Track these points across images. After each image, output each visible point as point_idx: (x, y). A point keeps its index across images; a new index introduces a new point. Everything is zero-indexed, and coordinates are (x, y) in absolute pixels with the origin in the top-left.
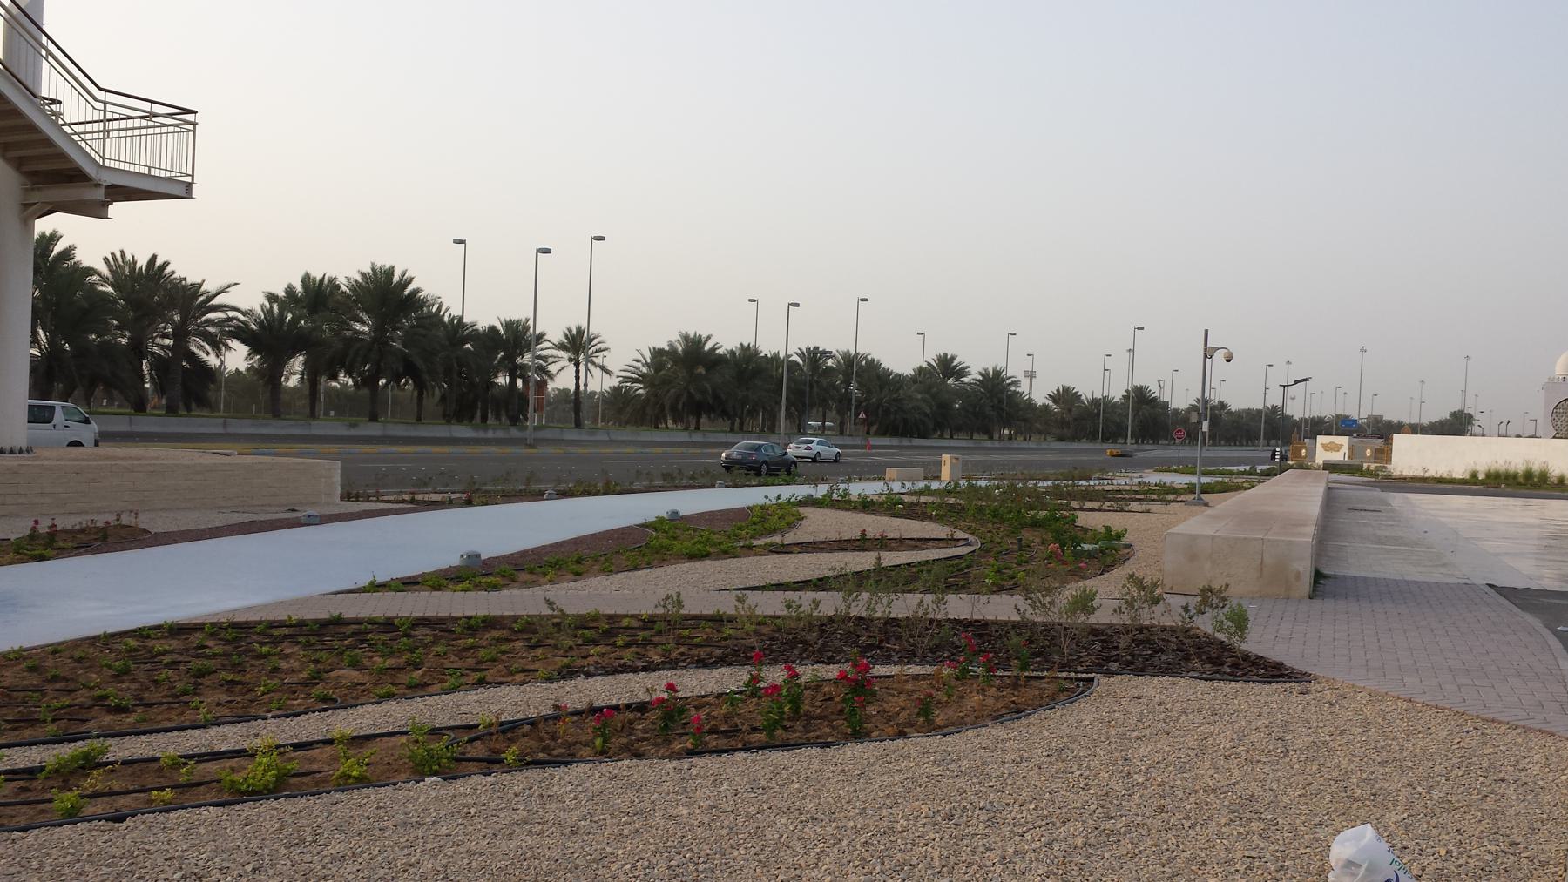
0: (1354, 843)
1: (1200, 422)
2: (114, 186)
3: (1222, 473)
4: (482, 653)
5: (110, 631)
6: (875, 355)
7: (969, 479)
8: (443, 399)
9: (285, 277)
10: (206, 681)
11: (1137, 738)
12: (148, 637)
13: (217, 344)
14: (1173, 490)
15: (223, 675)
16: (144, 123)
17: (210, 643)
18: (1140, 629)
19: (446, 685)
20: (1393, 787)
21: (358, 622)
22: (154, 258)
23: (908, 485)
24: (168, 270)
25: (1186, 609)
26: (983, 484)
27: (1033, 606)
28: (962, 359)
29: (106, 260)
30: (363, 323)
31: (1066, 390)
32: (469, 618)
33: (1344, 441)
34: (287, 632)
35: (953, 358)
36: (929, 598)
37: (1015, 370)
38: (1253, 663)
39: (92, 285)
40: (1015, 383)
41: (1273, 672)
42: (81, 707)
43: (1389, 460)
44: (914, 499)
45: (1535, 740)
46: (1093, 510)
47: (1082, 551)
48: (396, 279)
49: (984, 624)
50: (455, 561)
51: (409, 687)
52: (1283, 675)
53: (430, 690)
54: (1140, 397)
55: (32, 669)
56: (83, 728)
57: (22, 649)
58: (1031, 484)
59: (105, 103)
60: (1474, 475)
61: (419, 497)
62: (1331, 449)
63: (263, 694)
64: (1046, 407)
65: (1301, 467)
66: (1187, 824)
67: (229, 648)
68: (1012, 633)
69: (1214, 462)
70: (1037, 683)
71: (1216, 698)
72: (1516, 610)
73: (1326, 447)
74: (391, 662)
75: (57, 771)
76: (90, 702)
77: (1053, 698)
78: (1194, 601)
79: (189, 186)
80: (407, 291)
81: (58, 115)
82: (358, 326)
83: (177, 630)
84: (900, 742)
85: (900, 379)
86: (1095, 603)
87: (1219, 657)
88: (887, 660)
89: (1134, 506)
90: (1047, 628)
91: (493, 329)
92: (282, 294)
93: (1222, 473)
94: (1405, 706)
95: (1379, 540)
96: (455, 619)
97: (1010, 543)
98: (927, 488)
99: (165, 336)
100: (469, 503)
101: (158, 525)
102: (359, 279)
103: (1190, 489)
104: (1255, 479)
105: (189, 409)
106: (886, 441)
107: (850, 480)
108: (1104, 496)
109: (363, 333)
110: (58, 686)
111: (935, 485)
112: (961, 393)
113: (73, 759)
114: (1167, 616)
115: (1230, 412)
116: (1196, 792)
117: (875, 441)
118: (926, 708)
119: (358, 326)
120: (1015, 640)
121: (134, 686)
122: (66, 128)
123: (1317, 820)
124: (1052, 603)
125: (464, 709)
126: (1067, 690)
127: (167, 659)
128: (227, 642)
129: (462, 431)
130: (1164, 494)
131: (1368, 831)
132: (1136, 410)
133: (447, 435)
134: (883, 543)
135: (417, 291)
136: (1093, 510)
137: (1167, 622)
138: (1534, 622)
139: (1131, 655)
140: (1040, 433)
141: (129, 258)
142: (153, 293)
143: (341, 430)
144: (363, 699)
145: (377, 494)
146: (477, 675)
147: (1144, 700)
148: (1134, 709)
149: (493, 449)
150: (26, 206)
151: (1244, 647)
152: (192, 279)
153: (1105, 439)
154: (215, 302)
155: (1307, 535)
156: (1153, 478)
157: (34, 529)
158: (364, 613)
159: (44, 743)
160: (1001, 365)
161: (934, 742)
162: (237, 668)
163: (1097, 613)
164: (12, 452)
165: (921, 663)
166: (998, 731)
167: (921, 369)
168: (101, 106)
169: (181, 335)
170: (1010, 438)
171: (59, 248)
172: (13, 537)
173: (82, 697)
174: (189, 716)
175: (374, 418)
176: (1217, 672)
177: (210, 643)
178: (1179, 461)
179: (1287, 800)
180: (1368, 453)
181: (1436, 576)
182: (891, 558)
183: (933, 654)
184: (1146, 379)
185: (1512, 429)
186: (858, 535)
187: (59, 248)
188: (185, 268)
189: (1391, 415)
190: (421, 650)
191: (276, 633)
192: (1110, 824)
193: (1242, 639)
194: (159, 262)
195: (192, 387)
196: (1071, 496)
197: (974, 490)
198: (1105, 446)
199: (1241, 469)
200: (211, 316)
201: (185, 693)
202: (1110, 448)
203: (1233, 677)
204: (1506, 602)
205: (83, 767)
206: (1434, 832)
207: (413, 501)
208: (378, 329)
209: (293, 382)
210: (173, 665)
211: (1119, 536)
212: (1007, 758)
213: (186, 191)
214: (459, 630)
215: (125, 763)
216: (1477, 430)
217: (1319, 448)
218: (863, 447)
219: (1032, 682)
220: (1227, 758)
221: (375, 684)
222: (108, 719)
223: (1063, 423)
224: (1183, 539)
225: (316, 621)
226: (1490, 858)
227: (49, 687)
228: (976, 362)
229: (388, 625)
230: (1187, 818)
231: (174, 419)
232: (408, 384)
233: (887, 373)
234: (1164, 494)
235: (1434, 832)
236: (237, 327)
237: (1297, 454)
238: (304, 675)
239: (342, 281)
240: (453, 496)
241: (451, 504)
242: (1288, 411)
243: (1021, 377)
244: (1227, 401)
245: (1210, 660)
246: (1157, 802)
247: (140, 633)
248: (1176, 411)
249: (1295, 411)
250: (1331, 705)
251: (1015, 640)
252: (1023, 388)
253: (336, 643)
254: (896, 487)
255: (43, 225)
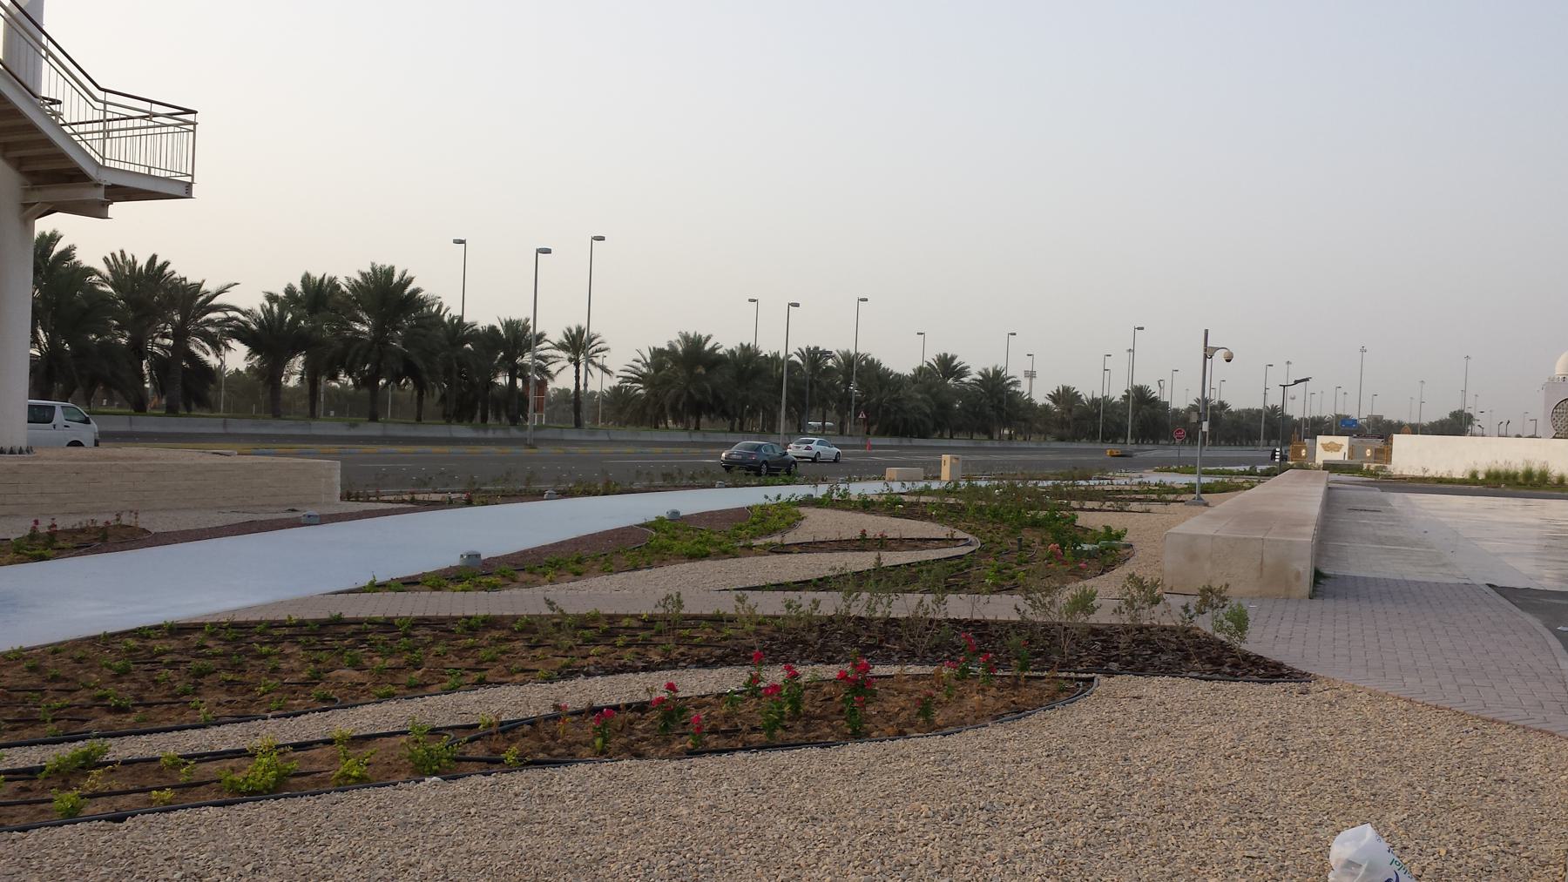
0: (1354, 843)
1: (1200, 422)
2: (114, 186)
3: (1222, 473)
4: (482, 653)
5: (110, 631)
6: (875, 355)
7: (969, 479)
8: (443, 399)
9: (285, 277)
10: (206, 681)
11: (1137, 738)
12: (148, 637)
13: (217, 344)
14: (1173, 490)
15: (223, 675)
16: (144, 123)
17: (210, 643)
18: (1140, 629)
19: (446, 685)
20: (1393, 787)
21: (358, 622)
22: (154, 258)
23: (908, 485)
24: (168, 270)
25: (1186, 609)
26: (983, 484)
27: (1033, 606)
28: (962, 359)
29: (106, 260)
30: (363, 323)
31: (1066, 390)
32: (469, 618)
33: (1344, 441)
34: (287, 632)
35: (953, 358)
36: (929, 598)
37: (1015, 370)
38: (1253, 663)
39: (92, 285)
40: (1015, 383)
41: (1273, 672)
42: (81, 707)
43: (1389, 460)
44: (914, 499)
45: (1535, 740)
46: (1093, 510)
47: (1082, 551)
48: (396, 279)
49: (984, 624)
50: (455, 561)
51: (409, 687)
52: (1283, 675)
53: (430, 690)
54: (1140, 397)
55: (32, 669)
56: (83, 728)
57: (22, 649)
58: (1031, 484)
59: (105, 103)
60: (1474, 475)
61: (419, 497)
62: (1331, 449)
63: (263, 694)
64: (1046, 407)
65: (1301, 467)
66: (1187, 824)
67: (229, 648)
68: (1012, 633)
69: (1214, 462)
70: (1037, 683)
71: (1216, 698)
72: (1516, 610)
73: (1326, 447)
74: (391, 662)
75: (57, 771)
76: (90, 702)
77: (1053, 698)
78: (1194, 601)
79: (189, 186)
80: (407, 291)
81: (58, 115)
82: (358, 326)
83: (177, 630)
84: (900, 742)
85: (900, 379)
86: (1095, 603)
87: (1219, 657)
88: (887, 660)
89: (1134, 506)
90: (1047, 628)
91: (493, 329)
92: (282, 294)
93: (1222, 473)
94: (1405, 706)
95: (1379, 540)
96: (455, 619)
97: (1010, 543)
98: (927, 488)
99: (165, 336)
100: (469, 503)
101: (158, 525)
102: (359, 279)
103: (1190, 489)
104: (1255, 479)
105: (189, 409)
106: (886, 441)
107: (850, 480)
108: (1104, 496)
109: (363, 333)
110: (58, 686)
111: (935, 485)
112: (961, 393)
113: (73, 759)
114: (1167, 616)
115: (1230, 412)
116: (1196, 792)
117: (875, 441)
118: (926, 708)
119: (358, 326)
120: (1015, 640)
121: (134, 686)
122: (66, 128)
123: (1317, 820)
124: (1052, 603)
125: (464, 709)
126: (1067, 690)
127: (167, 659)
128: (227, 642)
129: (462, 431)
130: (1164, 494)
131: (1368, 831)
132: (1136, 410)
133: (447, 435)
134: (883, 543)
135: (417, 291)
136: (1093, 510)
137: (1167, 622)
138: (1534, 622)
139: (1131, 655)
140: (1040, 433)
141: (129, 258)
142: (153, 293)
143: (341, 430)
144: (363, 699)
145: (377, 494)
146: (477, 675)
147: (1144, 700)
148: (1134, 709)
149: (493, 449)
150: (26, 206)
151: (1244, 647)
152: (192, 279)
153: (1105, 439)
154: (215, 302)
155: (1307, 535)
156: (1153, 478)
157: (34, 529)
158: (364, 613)
159: (44, 743)
160: (1001, 365)
161: (934, 742)
162: (237, 668)
163: (1097, 613)
164: (12, 452)
165: (921, 663)
166: (998, 731)
167: (921, 369)
168: (101, 106)
169: (181, 335)
170: (1010, 438)
171: (59, 248)
172: (13, 537)
173: (82, 697)
174: (189, 716)
175: (374, 418)
176: (1217, 672)
177: (210, 643)
178: (1179, 461)
179: (1287, 800)
180: (1368, 453)
181: (1436, 576)
182: (891, 558)
183: (933, 654)
184: (1146, 379)
185: (1512, 429)
186: (858, 535)
187: (59, 248)
188: (185, 268)
189: (1391, 415)
190: (421, 650)
191: (276, 633)
192: (1110, 824)
193: (1242, 639)
194: (159, 262)
195: (192, 387)
196: (1071, 496)
197: (974, 490)
198: (1105, 446)
199: (1241, 469)
200: (211, 316)
201: (185, 693)
202: (1110, 448)
203: (1233, 677)
204: (1506, 602)
205: (83, 767)
206: (1434, 832)
207: (413, 501)
208: (378, 329)
209: (293, 382)
210: (173, 665)
211: (1119, 536)
212: (1007, 758)
213: (186, 191)
214: (459, 630)
215: (125, 763)
216: (1477, 430)
217: (1319, 448)
218: (863, 447)
219: (1032, 682)
220: (1227, 758)
221: (375, 684)
222: (108, 719)
223: (1063, 423)
224: (1183, 539)
225: (316, 621)
226: (1490, 858)
227: (49, 687)
228: (976, 362)
229: (388, 625)
230: (1187, 818)
231: (174, 419)
232: (408, 384)
233: (887, 373)
234: (1164, 494)
235: (1434, 832)
236: (237, 327)
237: (1297, 454)
238: (304, 675)
239: (342, 281)
240: (453, 496)
241: (451, 504)
242: (1288, 411)
243: (1021, 377)
244: (1227, 401)
245: (1210, 660)
246: (1157, 802)
247: (140, 633)
248: (1176, 411)
249: (1295, 411)
250: (1331, 705)
251: (1015, 640)
252: (1023, 388)
253: (336, 643)
254: (896, 487)
255: (43, 225)
